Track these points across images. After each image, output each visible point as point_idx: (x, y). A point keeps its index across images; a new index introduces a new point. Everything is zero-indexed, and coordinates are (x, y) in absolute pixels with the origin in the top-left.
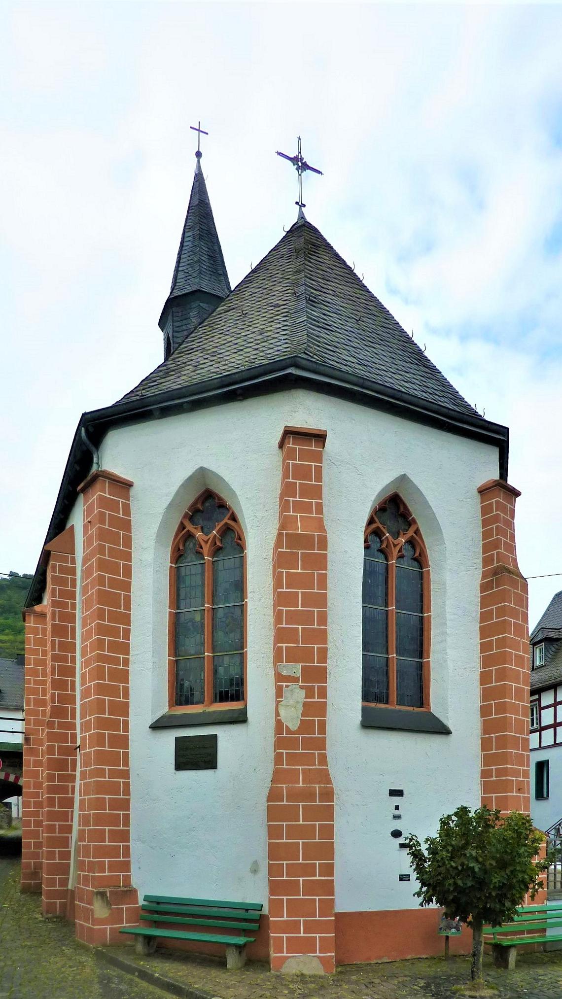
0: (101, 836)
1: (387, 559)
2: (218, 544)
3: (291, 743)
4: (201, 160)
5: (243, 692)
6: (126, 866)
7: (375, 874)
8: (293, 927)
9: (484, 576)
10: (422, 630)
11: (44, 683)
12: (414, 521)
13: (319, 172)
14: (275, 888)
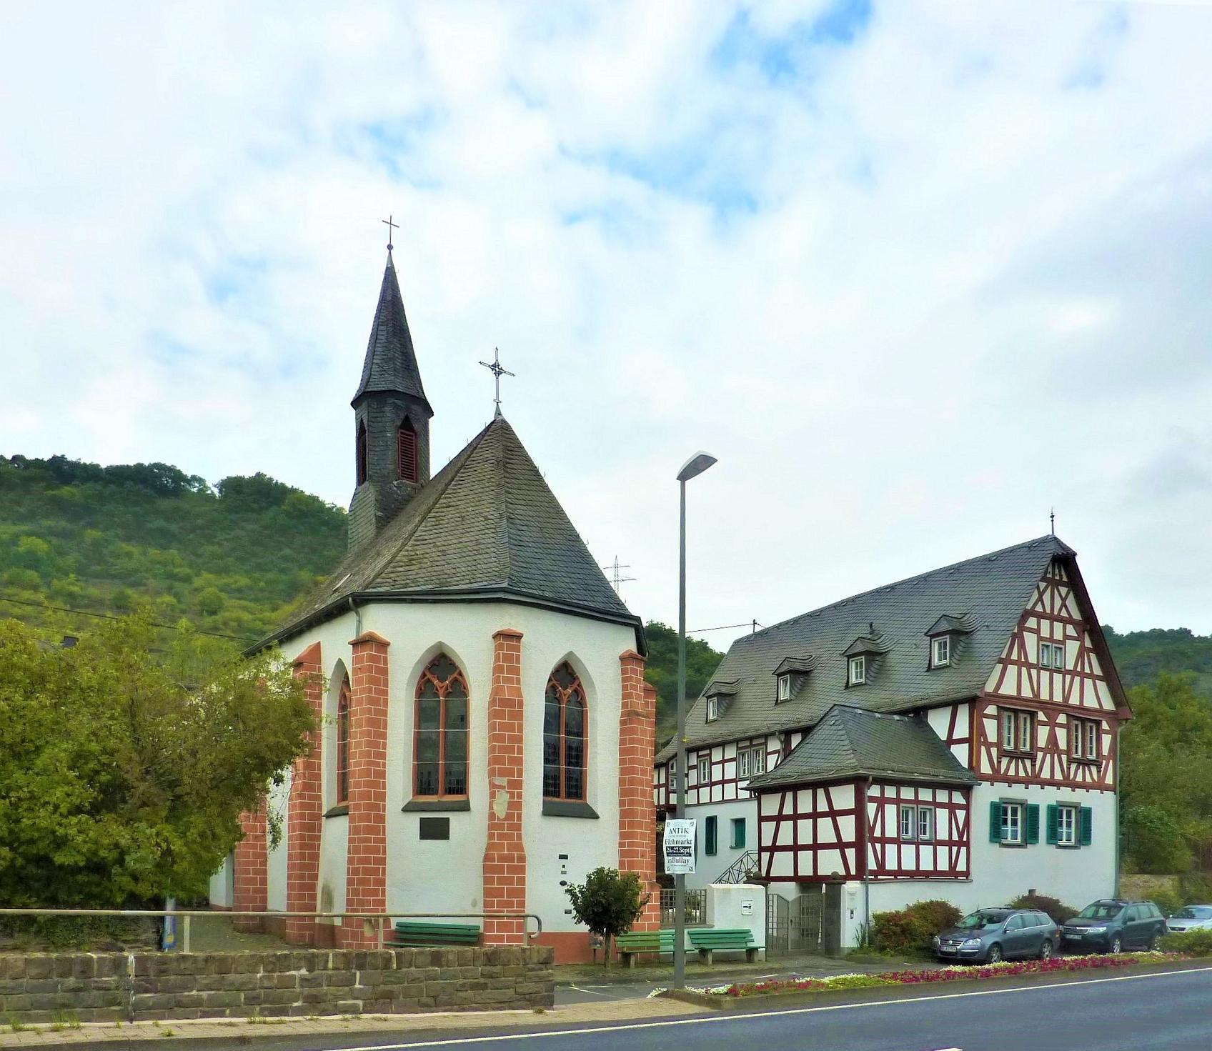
3: (501, 826)
7: (550, 906)
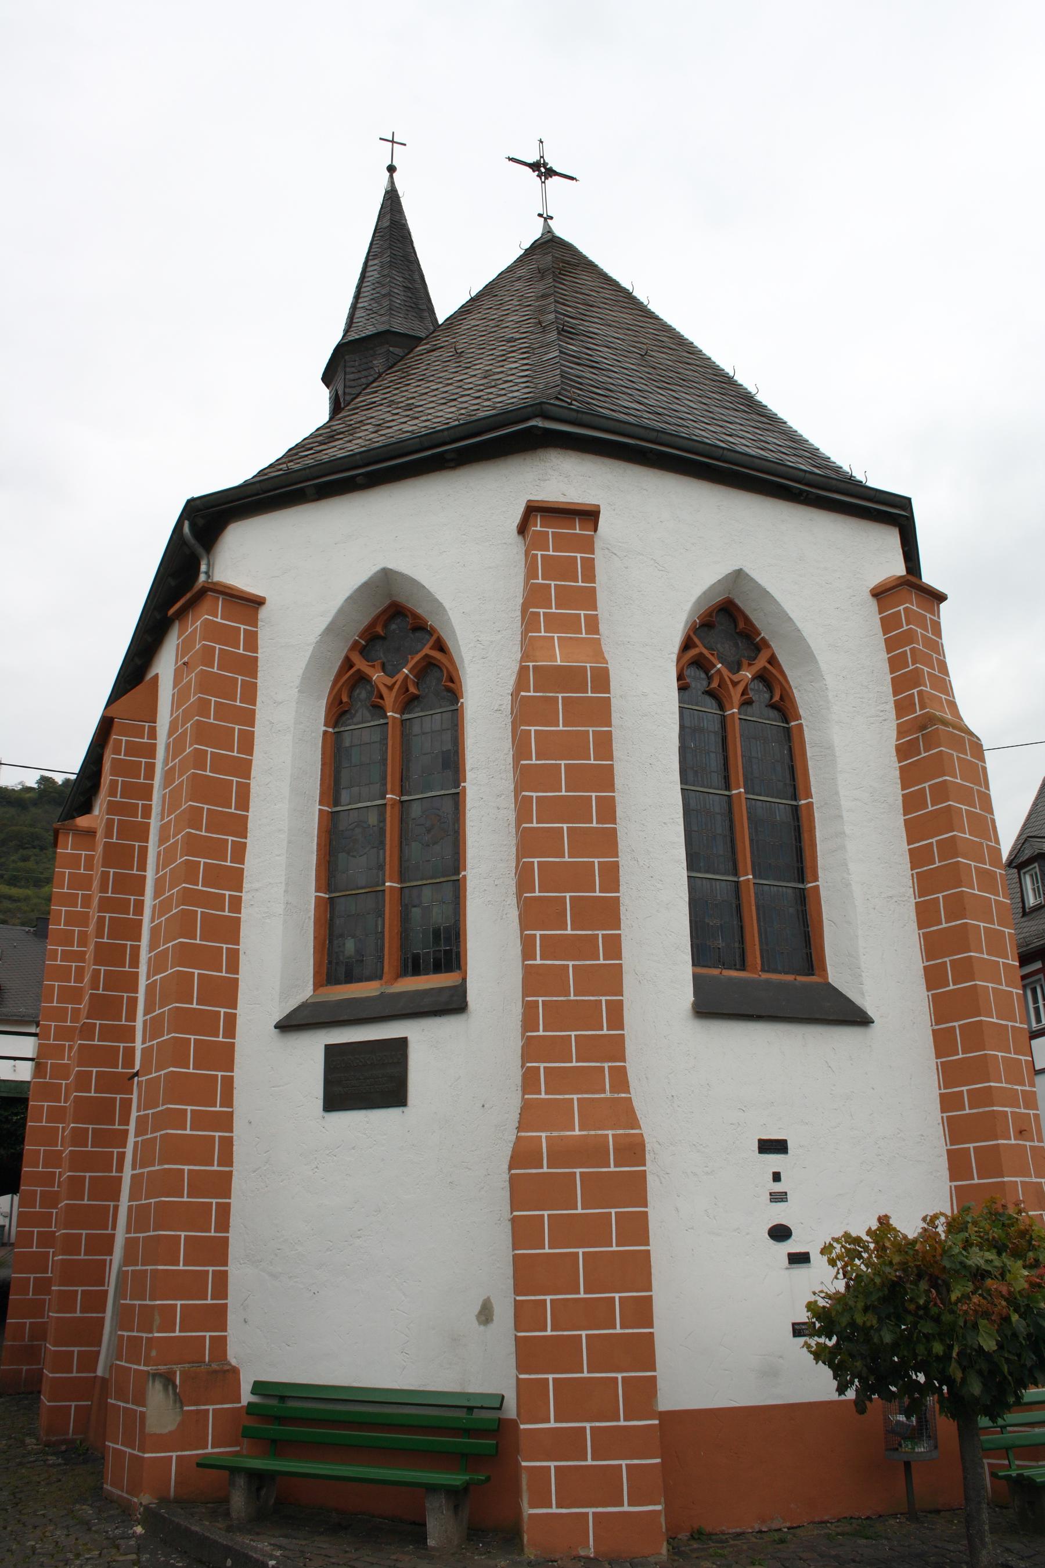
0: (168, 1250)
1: (722, 707)
2: (412, 689)
4: (395, 175)
5: (458, 954)
6: (218, 1317)
8: (568, 1444)
9: (901, 732)
10: (798, 830)
11: (80, 956)
12: (765, 644)
13: (572, 178)
14: (528, 1355)
